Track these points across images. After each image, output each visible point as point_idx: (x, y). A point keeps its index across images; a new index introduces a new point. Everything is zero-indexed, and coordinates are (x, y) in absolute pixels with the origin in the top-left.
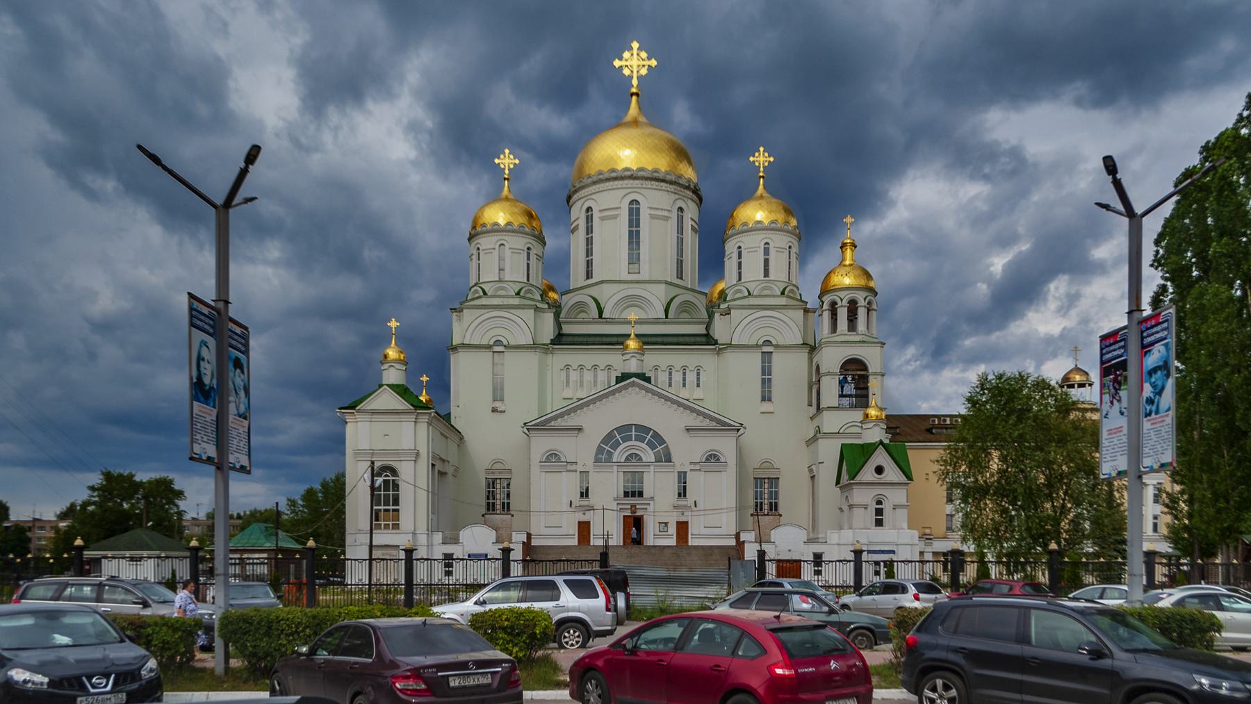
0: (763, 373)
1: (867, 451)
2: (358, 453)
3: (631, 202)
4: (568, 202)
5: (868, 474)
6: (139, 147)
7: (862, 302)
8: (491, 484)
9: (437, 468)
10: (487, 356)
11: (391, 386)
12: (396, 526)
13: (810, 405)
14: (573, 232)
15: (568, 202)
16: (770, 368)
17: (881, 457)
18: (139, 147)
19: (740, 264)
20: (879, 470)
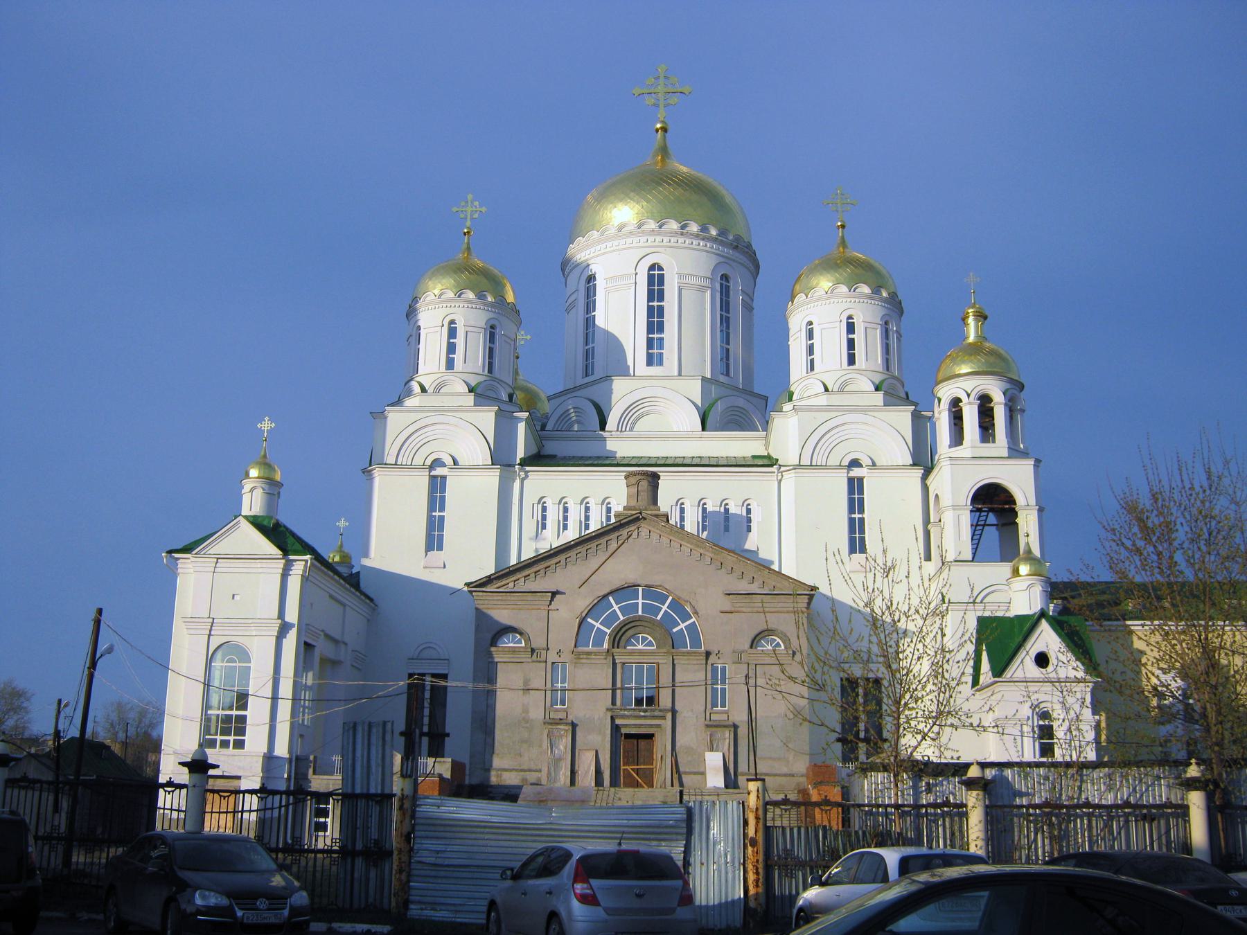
0: (851, 510)
1: (1025, 627)
2: (191, 621)
3: (652, 267)
4: (563, 271)
5: (1024, 665)
6: (100, 611)
7: (998, 398)
8: (415, 691)
9: (317, 653)
10: (610, 686)
11: (246, 517)
12: (240, 745)
13: (754, 457)
14: (568, 311)
15: (563, 271)
16: (861, 501)
17: (1046, 638)
18: (100, 611)
19: (811, 350)
20: (1042, 660)
